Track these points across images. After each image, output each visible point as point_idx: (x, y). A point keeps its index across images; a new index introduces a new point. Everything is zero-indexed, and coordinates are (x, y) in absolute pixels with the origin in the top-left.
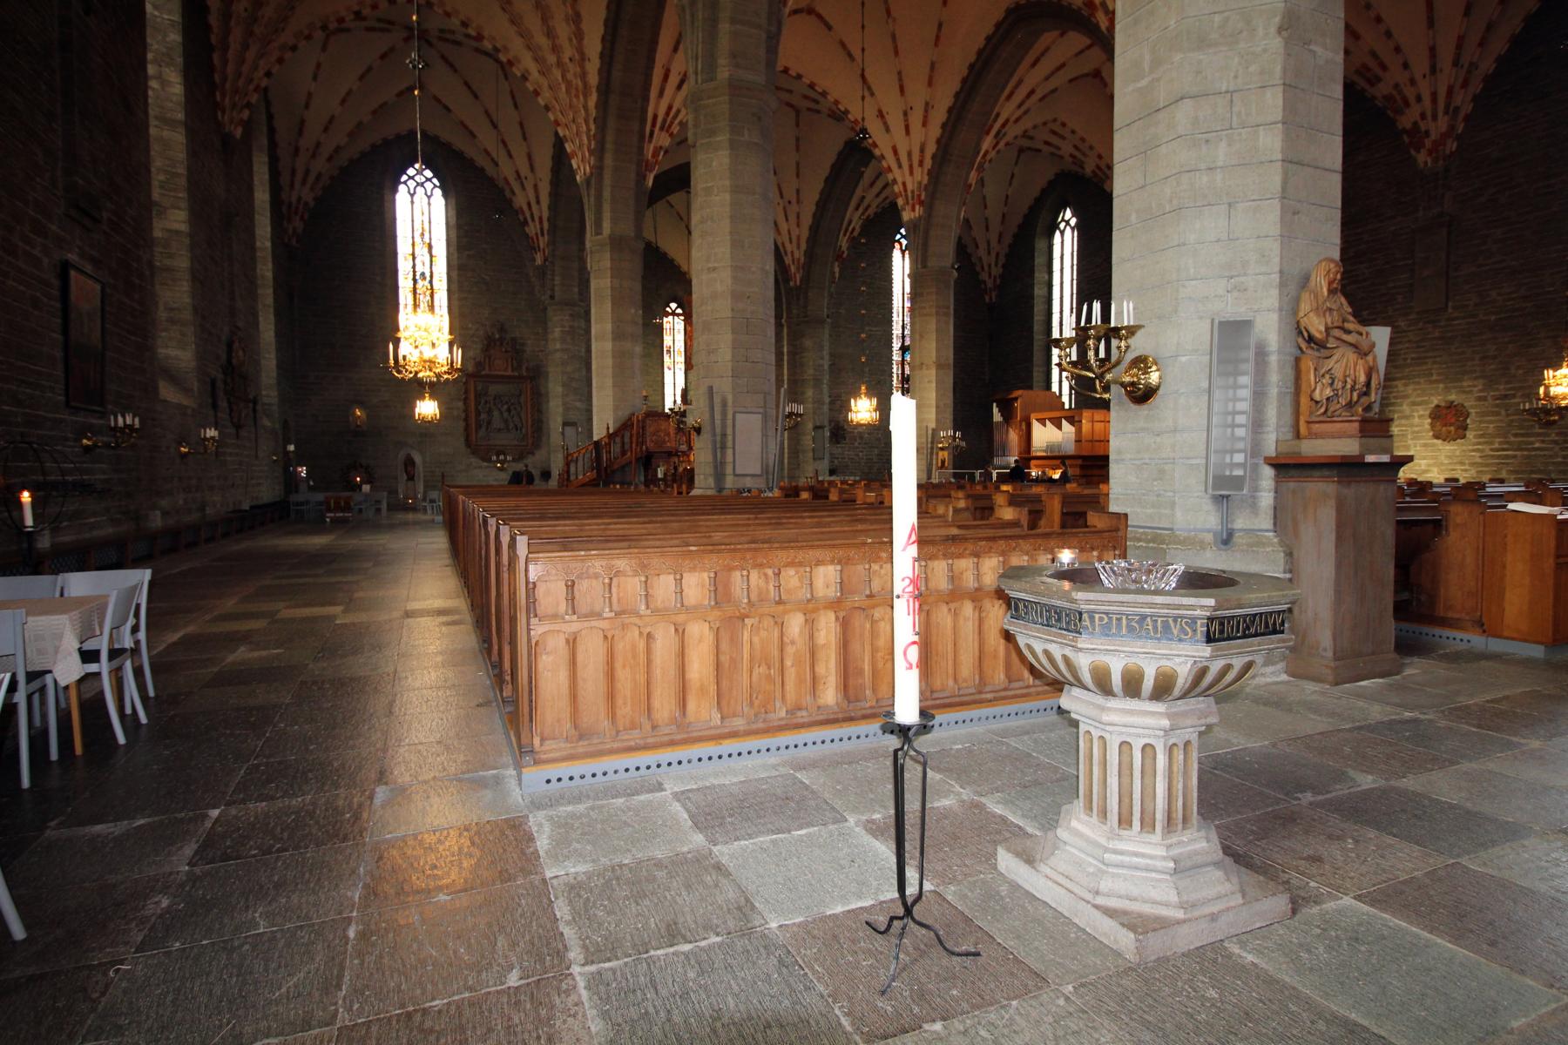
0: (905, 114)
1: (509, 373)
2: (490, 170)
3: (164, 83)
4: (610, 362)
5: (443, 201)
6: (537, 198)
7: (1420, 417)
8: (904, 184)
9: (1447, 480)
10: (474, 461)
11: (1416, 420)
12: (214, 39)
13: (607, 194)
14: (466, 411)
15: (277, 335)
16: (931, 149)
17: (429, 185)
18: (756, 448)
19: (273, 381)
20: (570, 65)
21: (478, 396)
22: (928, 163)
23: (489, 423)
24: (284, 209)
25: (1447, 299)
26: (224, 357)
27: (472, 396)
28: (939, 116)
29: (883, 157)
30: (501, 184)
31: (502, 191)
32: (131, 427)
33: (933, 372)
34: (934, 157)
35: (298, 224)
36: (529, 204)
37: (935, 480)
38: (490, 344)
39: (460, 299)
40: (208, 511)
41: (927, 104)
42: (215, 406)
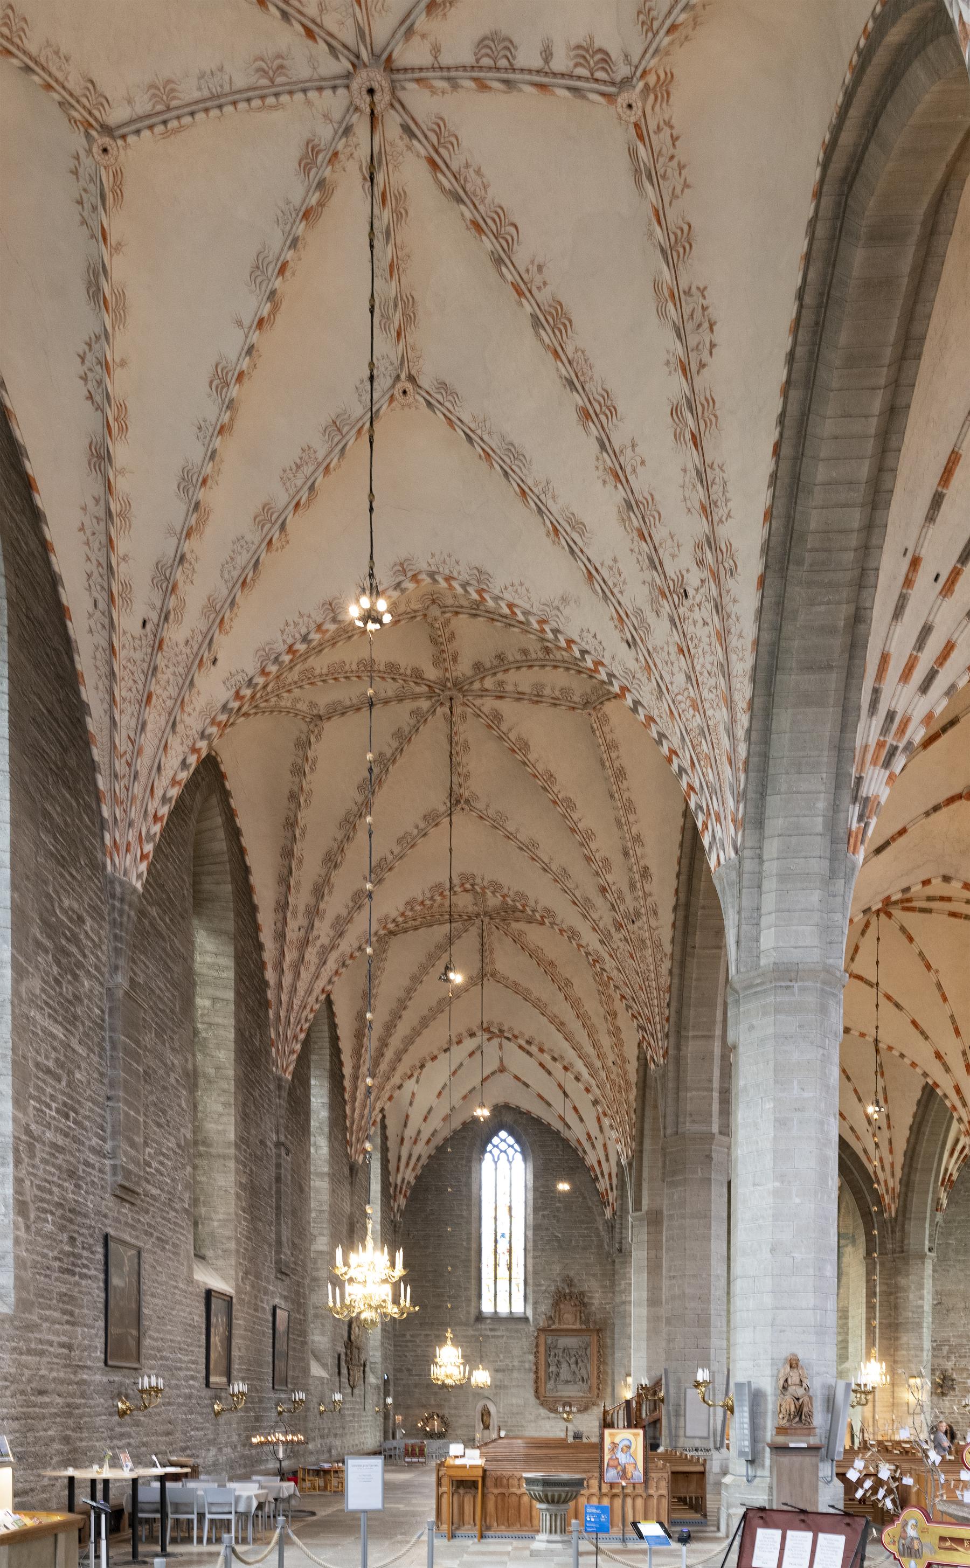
1: (578, 1326)
2: (566, 1134)
3: (317, 1148)
4: (645, 1326)
5: (522, 1165)
6: (607, 1156)
10: (543, 1412)
12: (347, 1096)
13: (645, 1174)
14: (536, 1364)
19: (378, 1343)
20: (614, 1069)
21: (549, 1349)
23: (558, 1375)
24: (392, 1190)
26: (346, 1335)
27: (542, 1349)
29: (946, 1096)
30: (573, 1144)
31: (575, 1151)
32: (301, 1400)
35: (402, 1201)
36: (599, 1162)
38: (559, 1298)
39: (535, 1257)
40: (333, 1452)
42: (339, 1373)
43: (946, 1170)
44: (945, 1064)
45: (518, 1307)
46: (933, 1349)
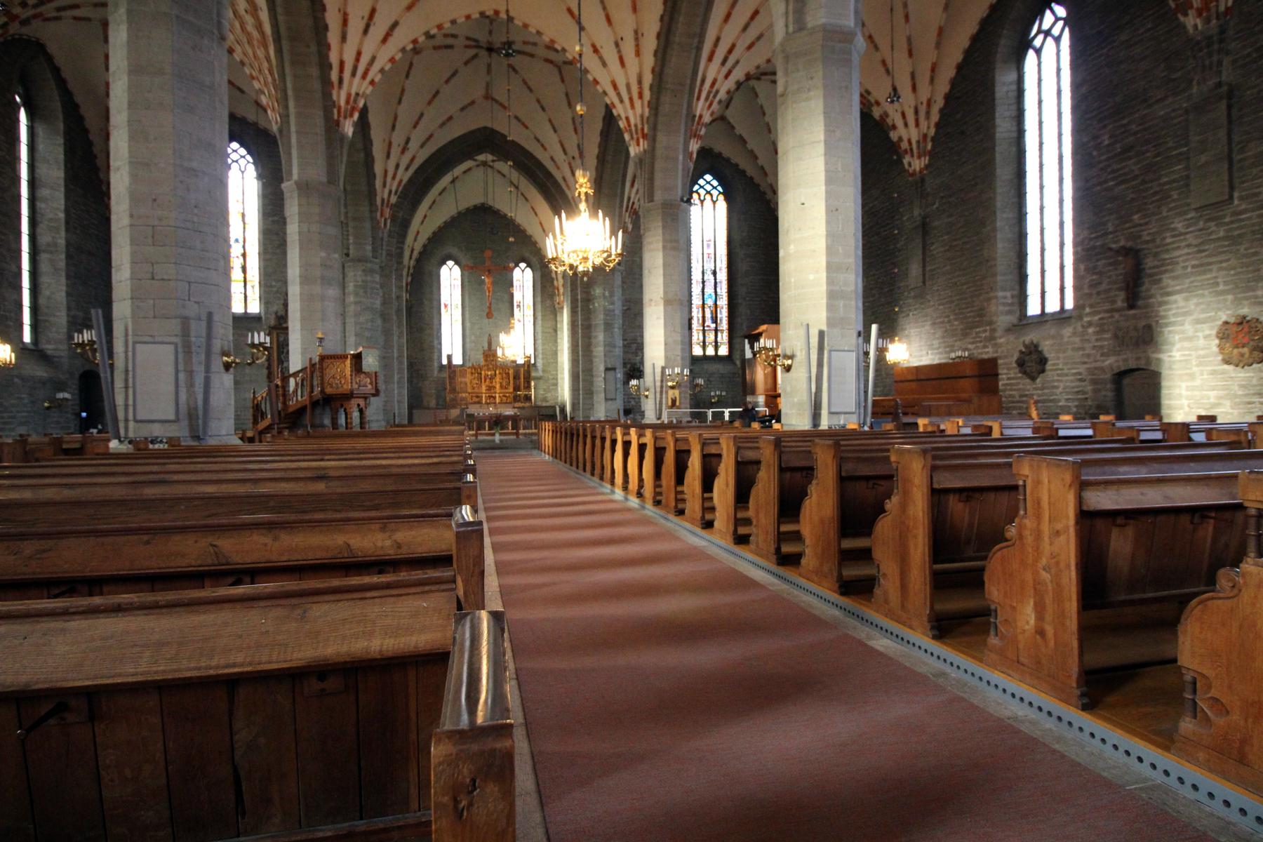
0: (617, 45)
7: (1206, 337)
8: (627, 118)
9: (1200, 418)
11: (1202, 342)
15: (68, 294)
16: (648, 79)
17: (242, 162)
18: (166, 385)
22: (647, 95)
25: (1232, 188)
28: (650, 44)
33: (661, 308)
34: (651, 87)
37: (665, 419)
41: (636, 32)
43: (629, 198)
44: (601, 58)
45: (254, 308)
46: (624, 346)
